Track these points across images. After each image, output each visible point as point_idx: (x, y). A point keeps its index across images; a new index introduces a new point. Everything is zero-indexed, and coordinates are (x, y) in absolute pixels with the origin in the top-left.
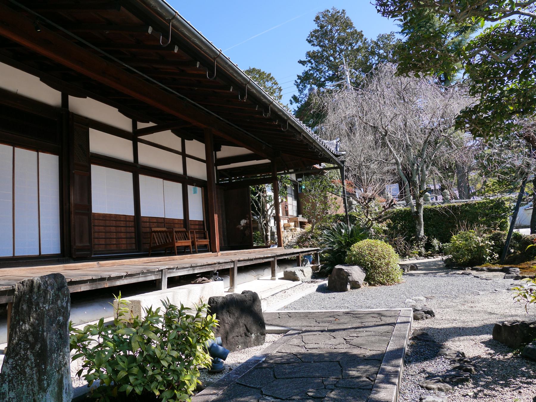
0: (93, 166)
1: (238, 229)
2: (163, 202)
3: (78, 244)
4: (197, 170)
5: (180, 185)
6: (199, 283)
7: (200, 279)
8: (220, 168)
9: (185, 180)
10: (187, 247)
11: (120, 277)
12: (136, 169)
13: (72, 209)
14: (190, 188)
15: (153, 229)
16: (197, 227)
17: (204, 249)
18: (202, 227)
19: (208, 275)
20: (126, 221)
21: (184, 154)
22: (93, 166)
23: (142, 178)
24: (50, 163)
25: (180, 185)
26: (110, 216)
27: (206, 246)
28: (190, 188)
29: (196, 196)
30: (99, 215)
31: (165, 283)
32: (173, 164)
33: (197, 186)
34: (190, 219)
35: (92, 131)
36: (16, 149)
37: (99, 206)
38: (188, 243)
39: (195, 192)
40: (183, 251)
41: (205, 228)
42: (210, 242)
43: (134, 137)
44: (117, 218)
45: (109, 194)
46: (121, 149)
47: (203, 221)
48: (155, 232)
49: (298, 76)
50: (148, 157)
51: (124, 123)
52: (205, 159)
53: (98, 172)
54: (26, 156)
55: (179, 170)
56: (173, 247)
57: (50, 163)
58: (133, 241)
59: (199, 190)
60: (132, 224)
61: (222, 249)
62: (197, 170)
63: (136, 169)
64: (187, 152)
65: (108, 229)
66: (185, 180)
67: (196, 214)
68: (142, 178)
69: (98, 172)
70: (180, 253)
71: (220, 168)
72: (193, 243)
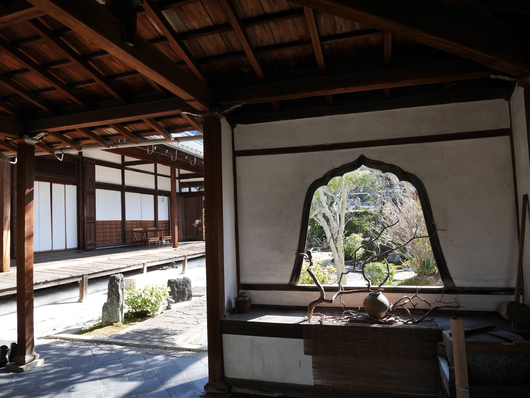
0: (97, 190)
1: (194, 226)
2: (141, 210)
3: (89, 242)
4: (165, 184)
6: (164, 270)
7: (164, 267)
8: (182, 181)
9: (156, 193)
11: (134, 265)
12: (123, 189)
13: (85, 220)
14: (159, 198)
15: (148, 229)
16: (164, 225)
18: (167, 225)
19: (170, 265)
20: (116, 224)
21: (156, 174)
22: (97, 190)
23: (127, 194)
24: (72, 190)
26: (106, 222)
28: (159, 198)
29: (163, 202)
30: (100, 222)
32: (148, 182)
33: (165, 196)
34: (99, 217)
35: (97, 167)
36: (54, 185)
38: (157, 239)
39: (163, 201)
41: (168, 227)
43: (122, 167)
44: (110, 223)
45: (107, 208)
46: (112, 176)
47: (169, 221)
48: (135, 231)
50: (133, 179)
51: (116, 158)
52: (170, 175)
53: (99, 193)
54: (58, 188)
55: (153, 187)
57: (72, 190)
58: (120, 237)
59: (166, 199)
60: (120, 226)
62: (165, 184)
63: (123, 189)
64: (159, 172)
65: (105, 230)
66: (156, 193)
67: (163, 216)
68: (127, 194)
69: (99, 193)
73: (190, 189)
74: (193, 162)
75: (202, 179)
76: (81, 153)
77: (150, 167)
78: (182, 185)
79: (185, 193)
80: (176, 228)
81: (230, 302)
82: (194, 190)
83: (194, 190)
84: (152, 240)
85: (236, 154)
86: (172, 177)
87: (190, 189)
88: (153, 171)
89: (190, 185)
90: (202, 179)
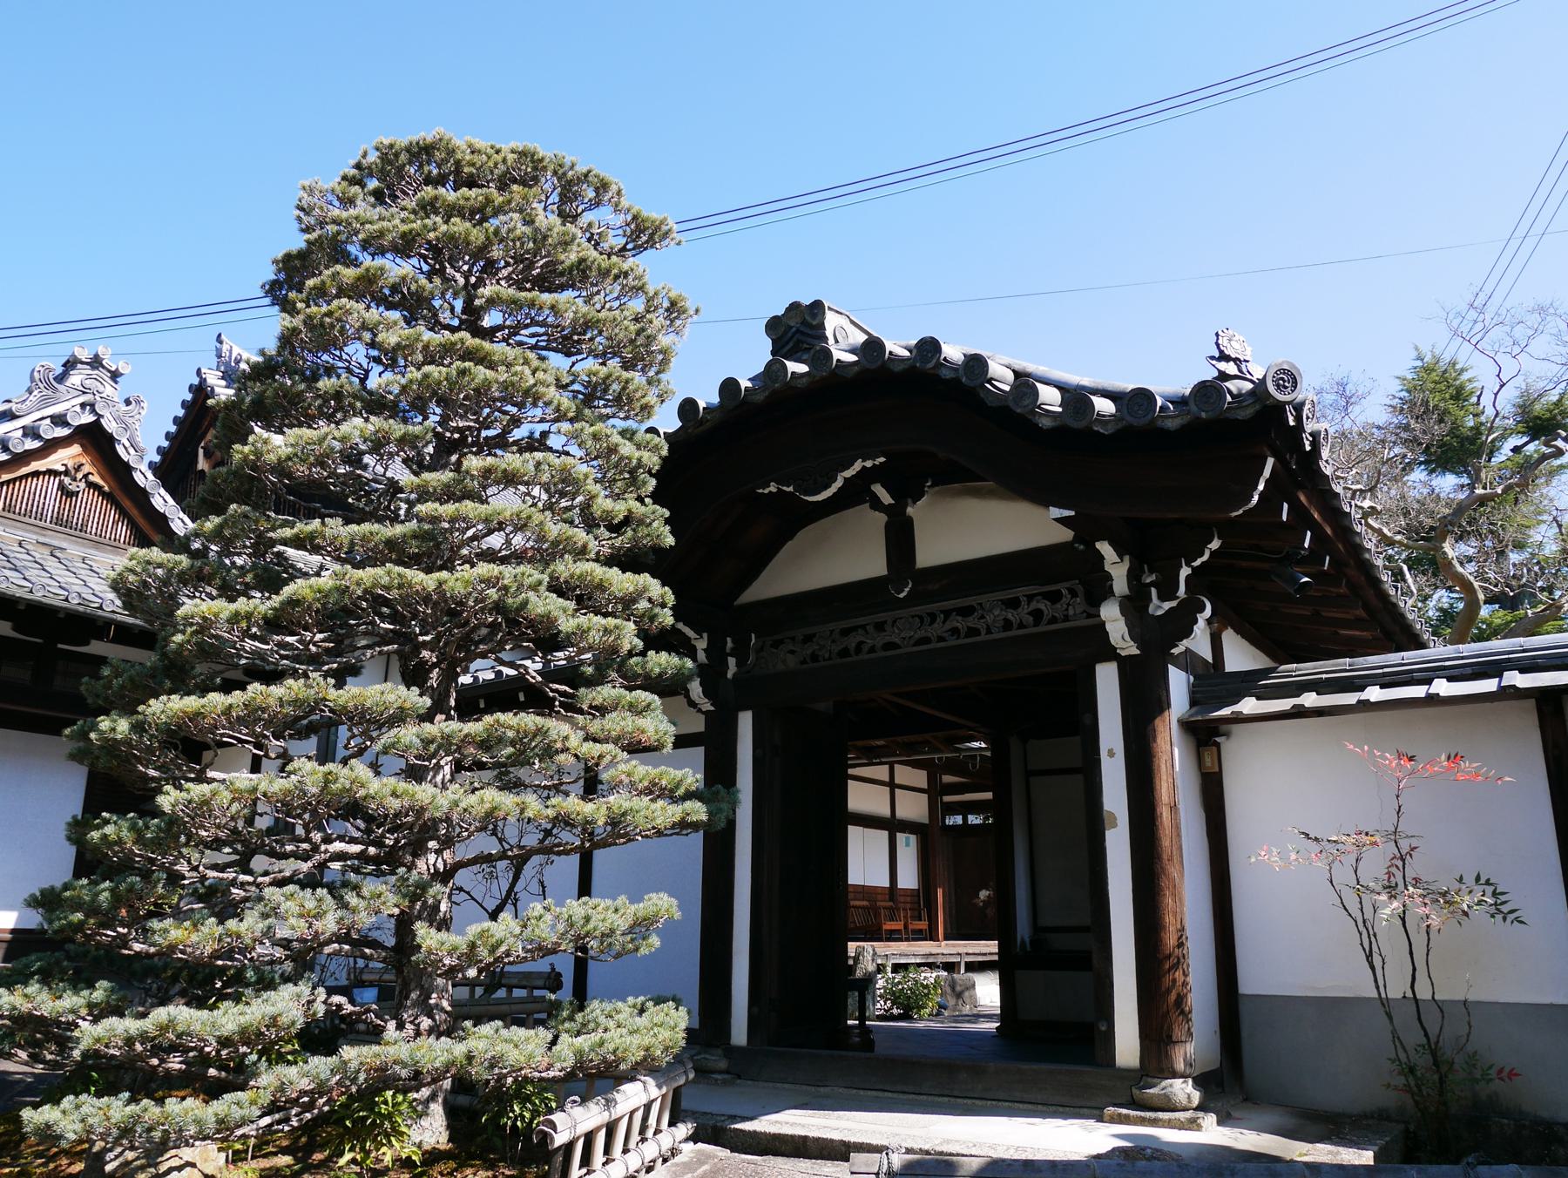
4: (913, 807)
5: (885, 834)
8: (947, 799)
10: (899, 931)
14: (901, 837)
17: (919, 936)
21: (892, 785)
25: (885, 834)
27: (920, 931)
28: (901, 837)
29: (908, 850)
31: (531, 1021)
37: (855, 877)
39: (907, 845)
40: (892, 936)
42: (930, 926)
49: (344, 178)
53: (854, 832)
55: (885, 811)
56: (880, 928)
59: (913, 838)
61: (946, 939)
62: (913, 807)
64: (897, 781)
67: (908, 878)
69: (854, 832)
70: (888, 940)
71: (947, 799)
72: (906, 927)
73: (965, 819)
74: (974, 766)
75: (989, 795)
76: (476, 678)
77: (881, 772)
78: (952, 809)
79: (955, 827)
80: (940, 891)
81: (1023, 941)
82: (973, 819)
83: (973, 819)
84: (889, 926)
85: (1029, 774)
86: (934, 791)
87: (965, 819)
88: (886, 778)
89: (966, 808)
90: (989, 795)
